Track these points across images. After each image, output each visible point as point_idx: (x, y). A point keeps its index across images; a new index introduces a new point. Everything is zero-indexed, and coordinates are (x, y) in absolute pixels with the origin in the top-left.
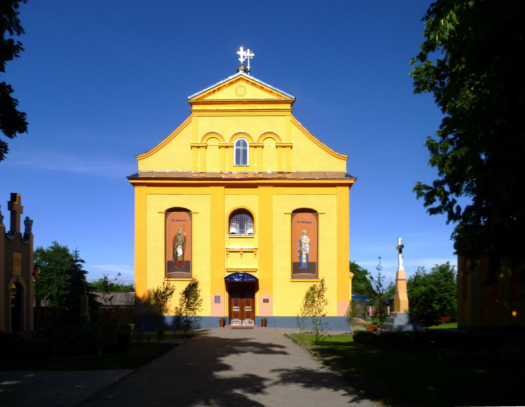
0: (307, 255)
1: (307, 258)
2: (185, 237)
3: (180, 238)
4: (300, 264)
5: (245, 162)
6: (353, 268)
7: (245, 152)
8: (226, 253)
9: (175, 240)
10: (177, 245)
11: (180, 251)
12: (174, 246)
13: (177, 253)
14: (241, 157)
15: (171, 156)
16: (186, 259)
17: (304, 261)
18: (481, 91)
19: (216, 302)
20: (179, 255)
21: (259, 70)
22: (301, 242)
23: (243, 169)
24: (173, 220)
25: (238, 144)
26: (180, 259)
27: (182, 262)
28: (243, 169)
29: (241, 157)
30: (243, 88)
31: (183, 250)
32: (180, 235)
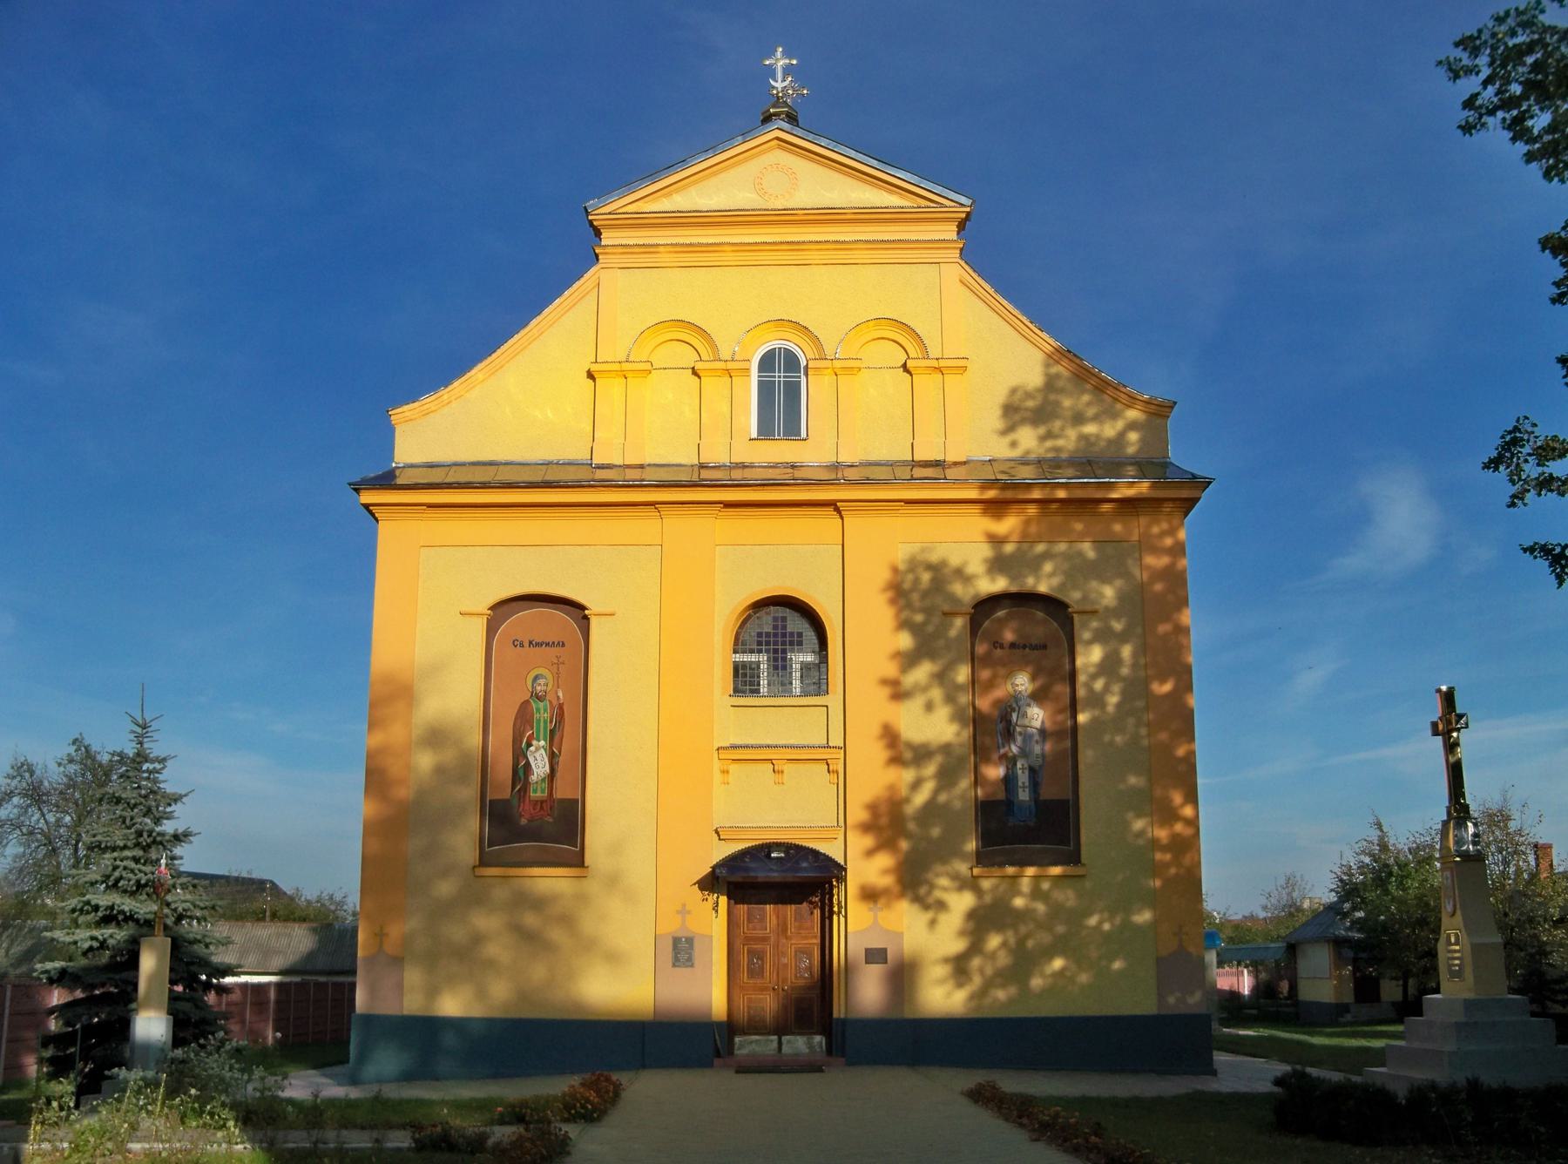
0: (1032, 770)
1: (1035, 784)
2: (561, 707)
3: (542, 713)
4: (1009, 804)
5: (792, 430)
6: (1530, 550)
7: (793, 391)
8: (717, 765)
9: (524, 717)
10: (531, 738)
11: (539, 764)
12: (517, 740)
13: (528, 765)
14: (781, 402)
15: (520, 398)
16: (563, 791)
17: (1024, 795)
18: (1038, 697)
19: (676, 962)
20: (534, 778)
21: (817, 120)
22: (1009, 722)
23: (780, 451)
24: (517, 644)
25: (767, 362)
26: (537, 793)
27: (549, 803)
28: (780, 451)
29: (781, 402)
30: (768, 174)
31: (553, 757)
32: (539, 698)
